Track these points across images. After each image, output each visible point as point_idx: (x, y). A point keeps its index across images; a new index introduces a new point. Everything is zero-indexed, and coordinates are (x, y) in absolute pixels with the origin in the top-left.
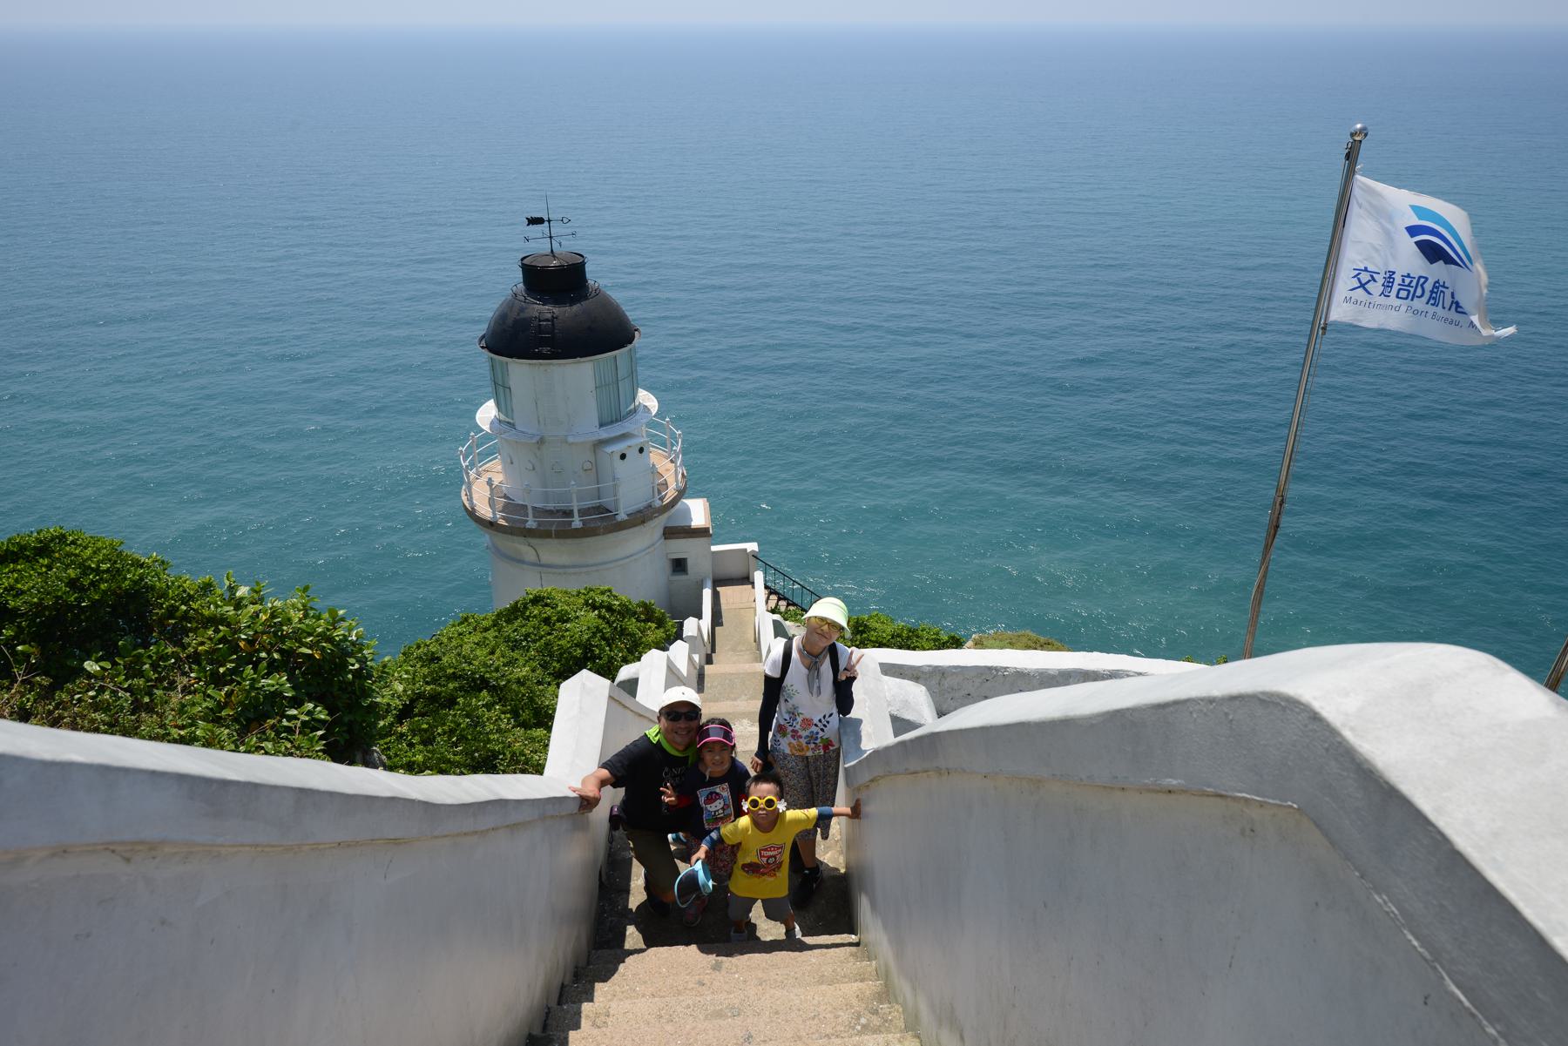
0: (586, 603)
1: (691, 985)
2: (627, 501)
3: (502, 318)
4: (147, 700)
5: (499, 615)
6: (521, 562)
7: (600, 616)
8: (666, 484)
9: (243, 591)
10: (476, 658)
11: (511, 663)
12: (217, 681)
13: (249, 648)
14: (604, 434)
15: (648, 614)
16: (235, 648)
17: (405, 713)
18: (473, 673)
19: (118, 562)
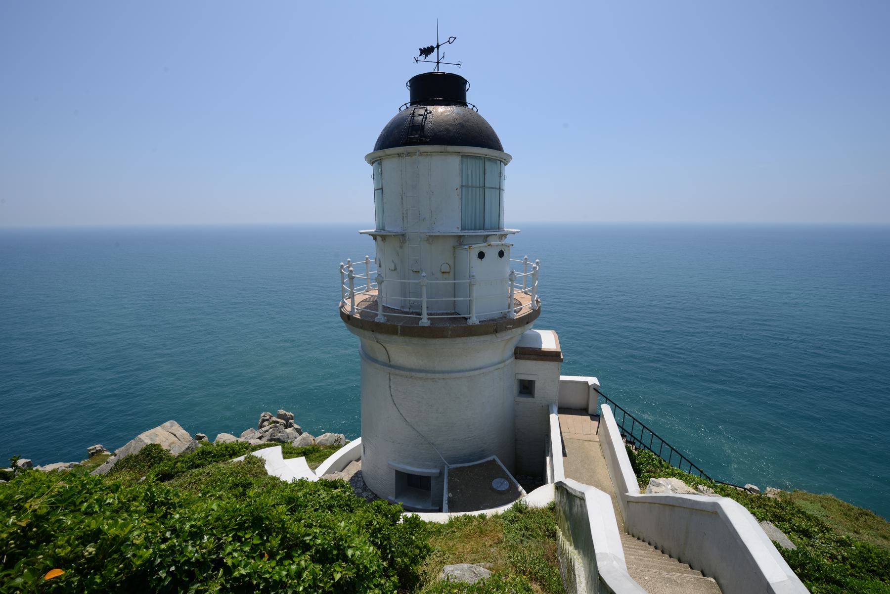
6: (375, 361)
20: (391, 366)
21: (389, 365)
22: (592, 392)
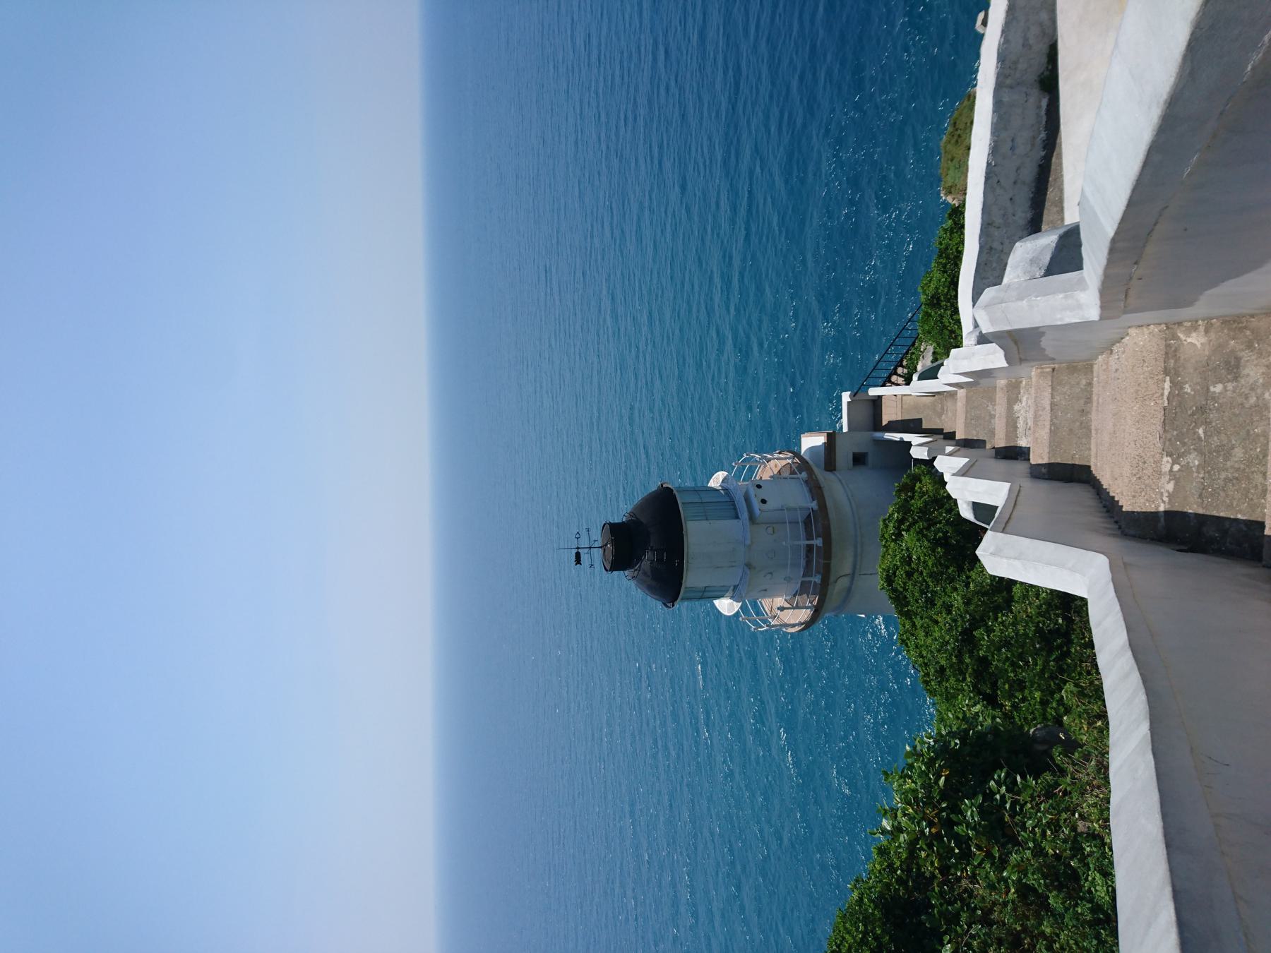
2: (798, 498)
4: (979, 912)
5: (901, 613)
6: (849, 590)
7: (908, 530)
9: (887, 824)
10: (942, 637)
11: (948, 608)
12: (966, 856)
14: (745, 515)
16: (938, 837)
17: (991, 701)
18: (957, 640)
19: (852, 915)
20: (854, 573)
21: (852, 576)
22: (857, 397)
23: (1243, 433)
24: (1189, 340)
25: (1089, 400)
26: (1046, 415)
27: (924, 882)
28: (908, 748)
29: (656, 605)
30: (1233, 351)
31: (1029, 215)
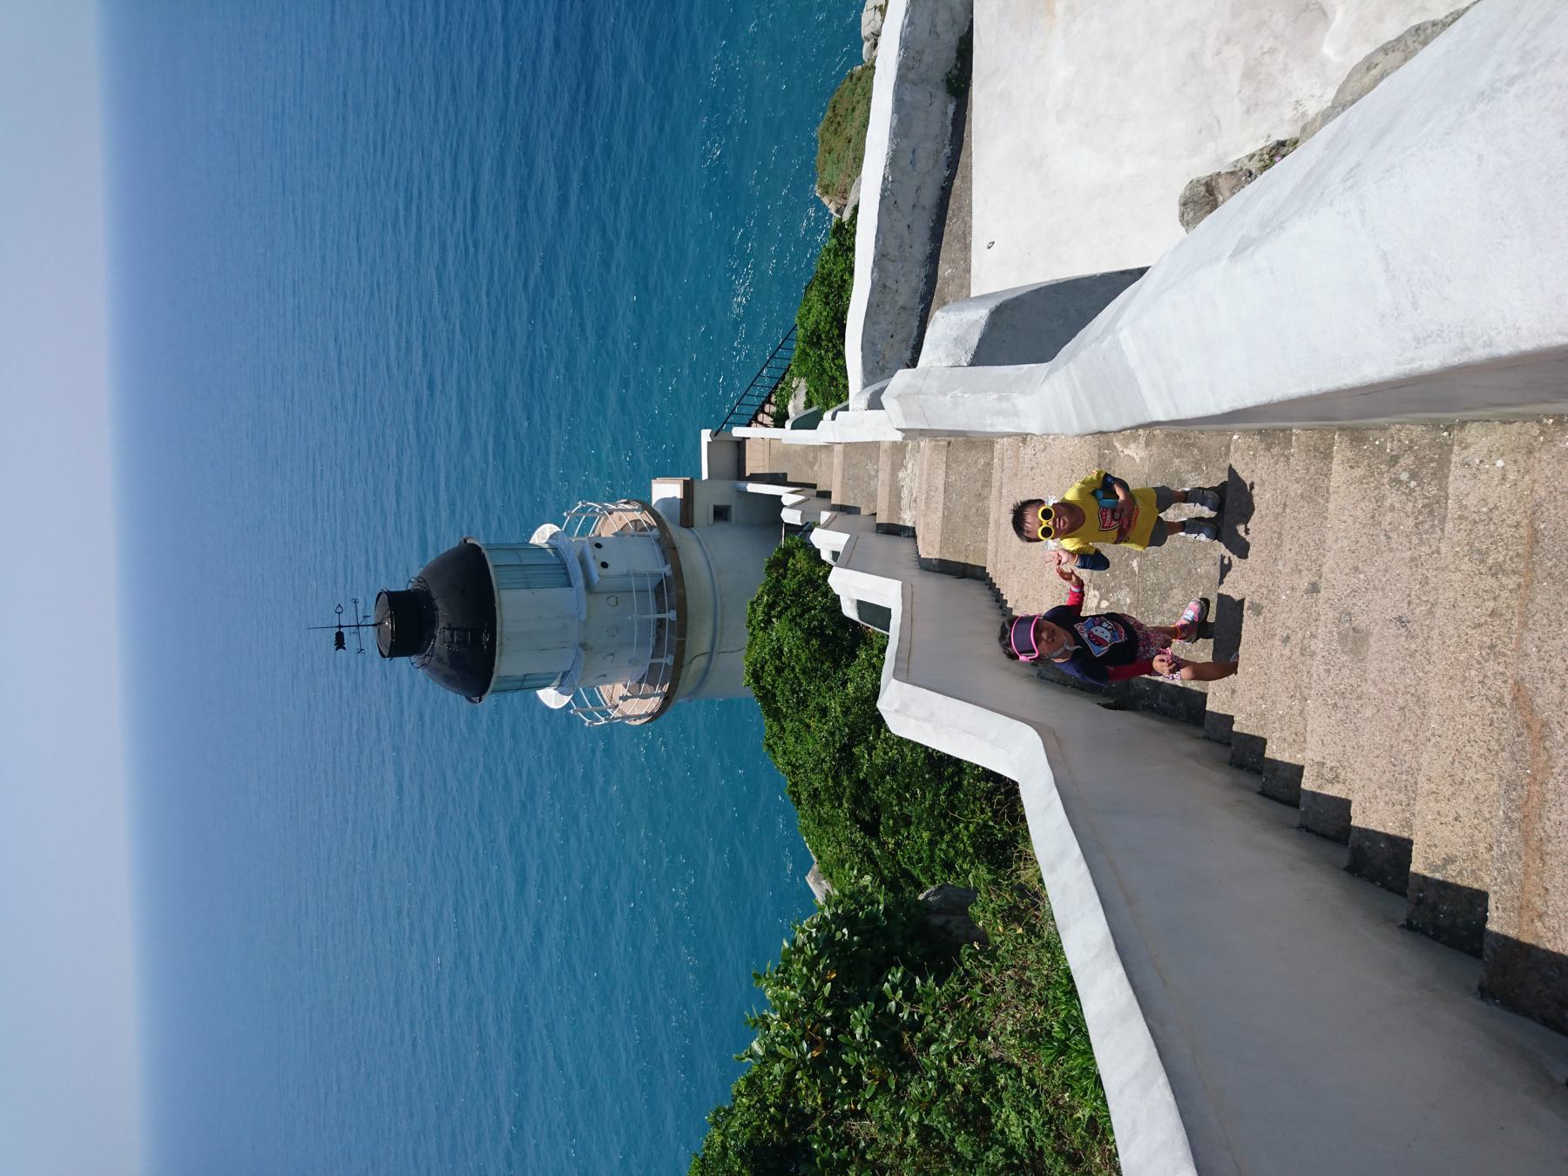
0: (764, 629)
1: (1287, 652)
2: (650, 563)
3: (449, 680)
6: (706, 672)
7: (779, 617)
8: (636, 522)
11: (824, 712)
12: (856, 1085)
13: (821, 1047)
14: (580, 583)
15: (779, 565)
20: (711, 653)
21: (710, 654)
22: (719, 437)
23: (1183, 572)
24: (1127, 452)
25: (987, 483)
26: (939, 497)
27: (802, 1119)
28: (786, 944)
29: (456, 701)
30: (1177, 472)
31: (928, 249)
